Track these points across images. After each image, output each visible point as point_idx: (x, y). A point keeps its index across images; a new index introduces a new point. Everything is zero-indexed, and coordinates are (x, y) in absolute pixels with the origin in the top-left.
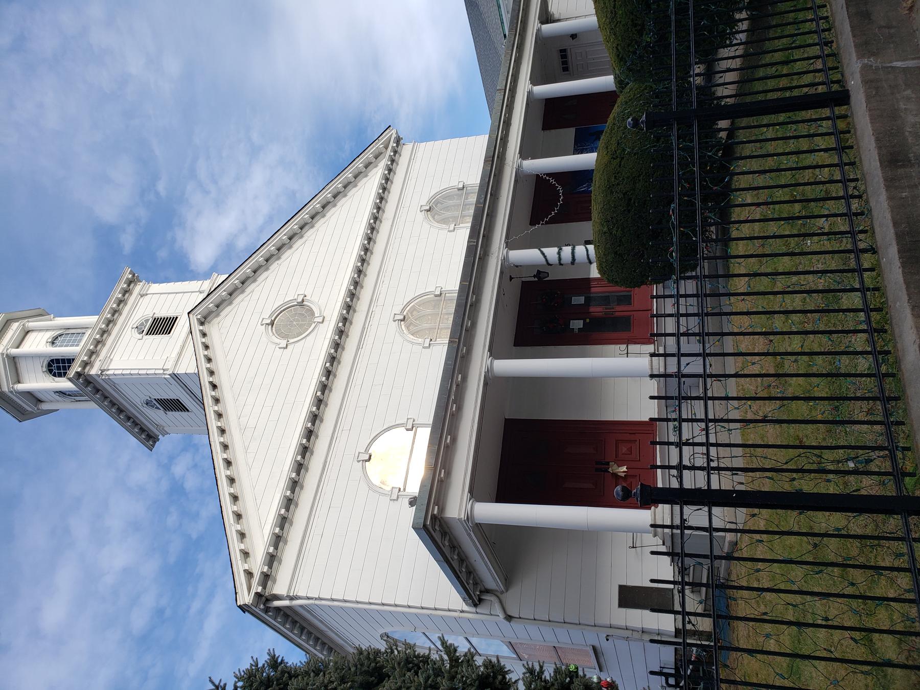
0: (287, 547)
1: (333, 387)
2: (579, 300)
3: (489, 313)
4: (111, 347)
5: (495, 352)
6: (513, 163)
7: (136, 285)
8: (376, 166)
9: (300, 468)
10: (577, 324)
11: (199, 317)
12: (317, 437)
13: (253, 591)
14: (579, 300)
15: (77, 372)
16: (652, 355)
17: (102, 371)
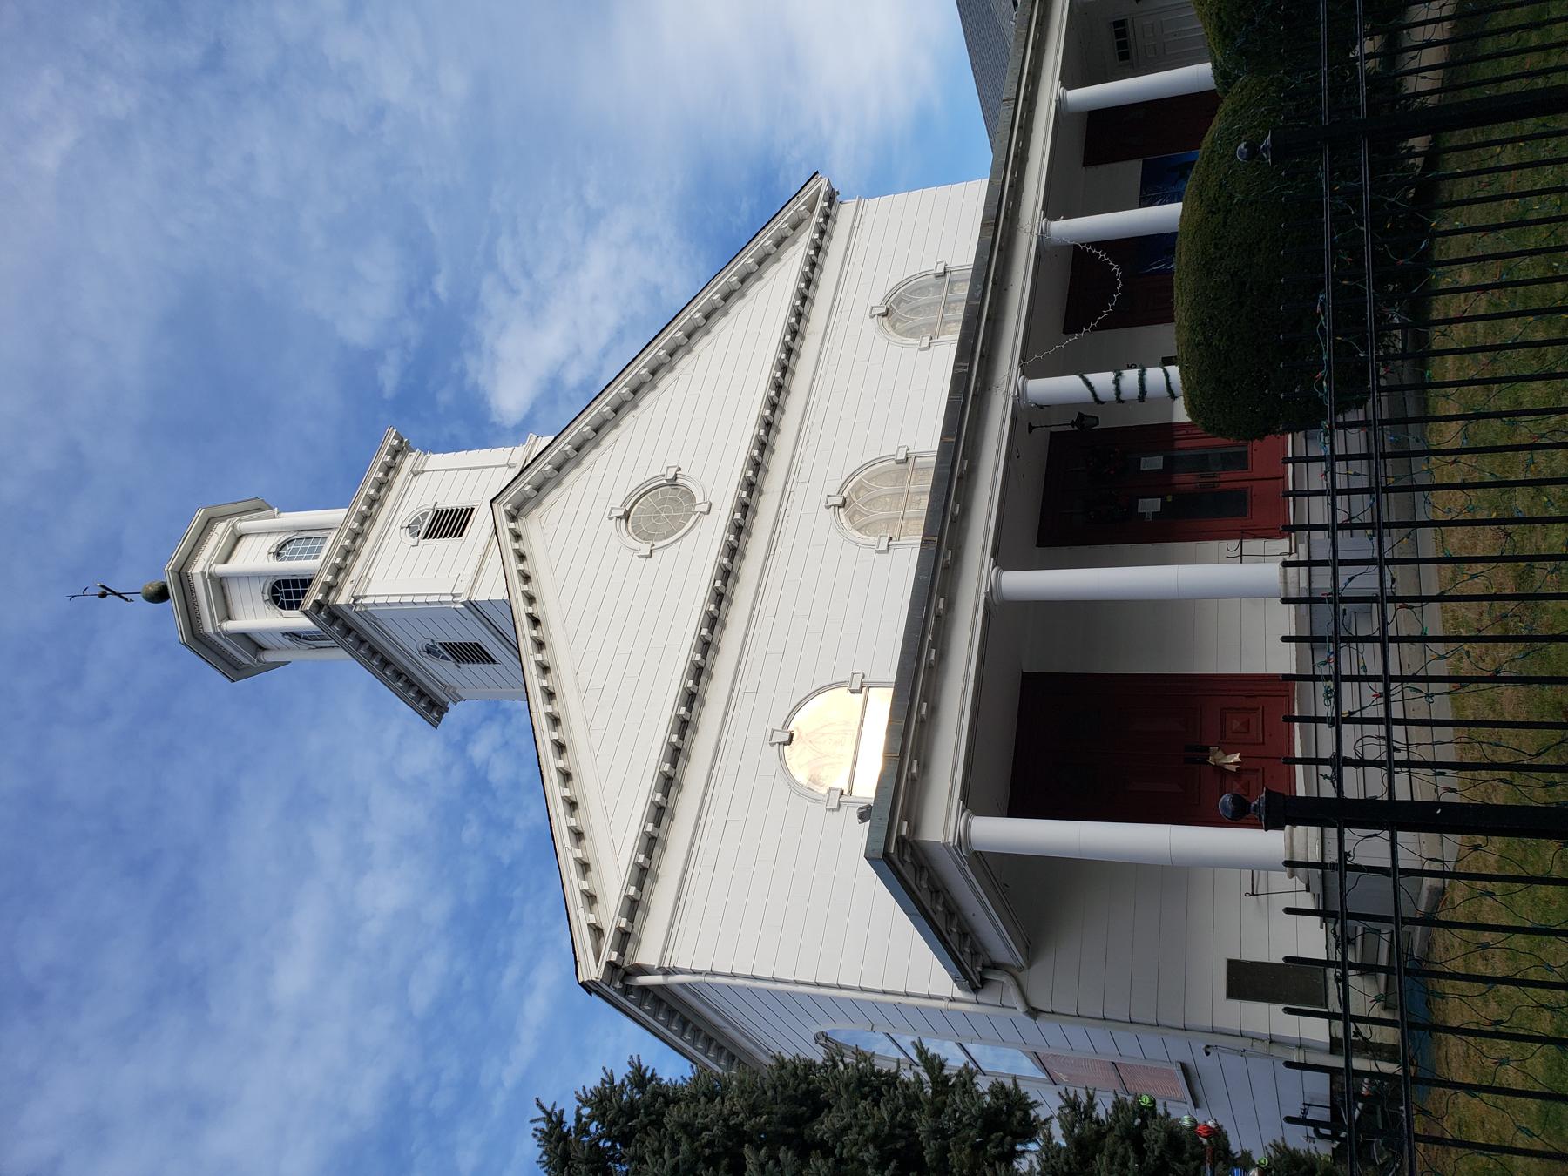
6: (1033, 226)
7: (405, 456)
8: (795, 243)
10: (1150, 506)
14: (1156, 462)
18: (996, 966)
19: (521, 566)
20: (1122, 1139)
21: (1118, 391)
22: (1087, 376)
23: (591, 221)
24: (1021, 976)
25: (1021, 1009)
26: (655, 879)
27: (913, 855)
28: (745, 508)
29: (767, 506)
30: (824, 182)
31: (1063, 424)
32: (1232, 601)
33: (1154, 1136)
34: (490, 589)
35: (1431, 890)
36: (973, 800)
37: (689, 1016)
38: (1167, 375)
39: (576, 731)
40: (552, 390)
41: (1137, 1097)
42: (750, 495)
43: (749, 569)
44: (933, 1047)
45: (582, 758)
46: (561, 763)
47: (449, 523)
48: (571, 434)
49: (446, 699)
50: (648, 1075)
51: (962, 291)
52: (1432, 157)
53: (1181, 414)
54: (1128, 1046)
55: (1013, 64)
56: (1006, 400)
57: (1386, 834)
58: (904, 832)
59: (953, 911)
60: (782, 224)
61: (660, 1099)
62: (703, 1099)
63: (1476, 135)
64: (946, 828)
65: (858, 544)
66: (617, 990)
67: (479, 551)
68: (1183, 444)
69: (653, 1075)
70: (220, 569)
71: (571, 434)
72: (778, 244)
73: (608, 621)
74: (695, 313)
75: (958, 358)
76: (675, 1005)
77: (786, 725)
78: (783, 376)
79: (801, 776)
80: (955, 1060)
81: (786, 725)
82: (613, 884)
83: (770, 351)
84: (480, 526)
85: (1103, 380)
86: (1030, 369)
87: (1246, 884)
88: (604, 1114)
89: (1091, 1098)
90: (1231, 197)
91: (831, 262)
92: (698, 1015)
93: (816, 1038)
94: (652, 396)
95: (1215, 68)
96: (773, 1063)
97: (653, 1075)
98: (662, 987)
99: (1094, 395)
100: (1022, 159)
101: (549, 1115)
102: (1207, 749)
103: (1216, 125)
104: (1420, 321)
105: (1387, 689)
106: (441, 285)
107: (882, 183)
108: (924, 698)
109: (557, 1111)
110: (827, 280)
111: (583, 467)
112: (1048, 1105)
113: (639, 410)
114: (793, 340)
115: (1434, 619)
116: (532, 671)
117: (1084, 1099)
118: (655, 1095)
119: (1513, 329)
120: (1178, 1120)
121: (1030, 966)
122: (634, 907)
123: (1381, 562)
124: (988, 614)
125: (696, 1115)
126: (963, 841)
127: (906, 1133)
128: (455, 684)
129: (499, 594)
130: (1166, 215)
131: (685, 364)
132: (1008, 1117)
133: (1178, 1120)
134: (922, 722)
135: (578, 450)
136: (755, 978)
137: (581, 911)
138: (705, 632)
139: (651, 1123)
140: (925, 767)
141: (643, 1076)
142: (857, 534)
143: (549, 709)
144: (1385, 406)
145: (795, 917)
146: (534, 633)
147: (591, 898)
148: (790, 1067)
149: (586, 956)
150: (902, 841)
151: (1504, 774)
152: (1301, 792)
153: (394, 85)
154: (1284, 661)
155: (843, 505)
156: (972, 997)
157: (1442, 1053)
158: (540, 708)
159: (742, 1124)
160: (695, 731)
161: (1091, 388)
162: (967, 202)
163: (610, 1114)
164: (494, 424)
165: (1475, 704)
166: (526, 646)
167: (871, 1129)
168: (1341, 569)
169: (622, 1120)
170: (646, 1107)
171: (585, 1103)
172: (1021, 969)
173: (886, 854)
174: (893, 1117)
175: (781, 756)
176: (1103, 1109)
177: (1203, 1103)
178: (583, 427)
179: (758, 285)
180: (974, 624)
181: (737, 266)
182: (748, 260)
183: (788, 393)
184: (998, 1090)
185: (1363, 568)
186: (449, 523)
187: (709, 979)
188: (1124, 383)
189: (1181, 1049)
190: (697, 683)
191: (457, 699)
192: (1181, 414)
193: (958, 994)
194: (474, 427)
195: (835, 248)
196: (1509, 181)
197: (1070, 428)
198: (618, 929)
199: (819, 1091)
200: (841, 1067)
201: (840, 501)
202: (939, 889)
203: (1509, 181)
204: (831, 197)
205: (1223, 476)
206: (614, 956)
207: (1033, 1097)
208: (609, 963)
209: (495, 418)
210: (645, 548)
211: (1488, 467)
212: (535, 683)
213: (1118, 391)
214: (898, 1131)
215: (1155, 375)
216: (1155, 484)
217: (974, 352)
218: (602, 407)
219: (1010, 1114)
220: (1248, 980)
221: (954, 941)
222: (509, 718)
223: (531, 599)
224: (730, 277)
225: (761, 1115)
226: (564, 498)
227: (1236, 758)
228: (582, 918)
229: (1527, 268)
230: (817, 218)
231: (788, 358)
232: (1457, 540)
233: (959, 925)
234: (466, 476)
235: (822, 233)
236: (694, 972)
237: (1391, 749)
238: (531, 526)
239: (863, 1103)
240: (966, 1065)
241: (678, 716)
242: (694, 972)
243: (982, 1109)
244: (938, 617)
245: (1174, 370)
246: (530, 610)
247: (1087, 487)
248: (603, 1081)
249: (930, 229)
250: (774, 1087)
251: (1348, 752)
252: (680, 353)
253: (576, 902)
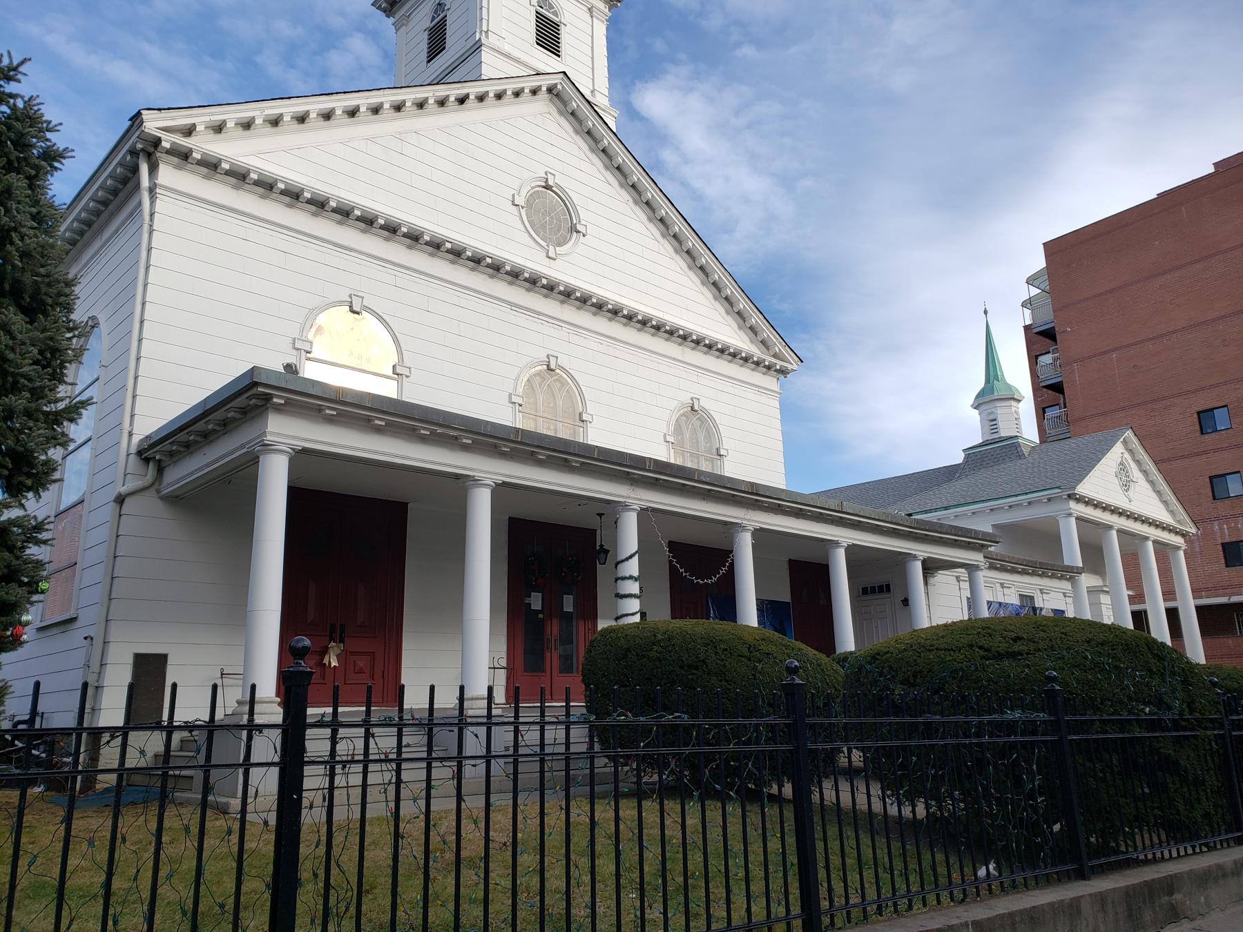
1: (319, 219)
2: (568, 604)
8: (752, 342)
14: (568, 604)
18: (160, 470)
19: (509, 93)
20: (8, 566)
21: (624, 578)
22: (637, 556)
23: (786, 181)
24: (153, 490)
25: (123, 490)
26: (236, 187)
27: (256, 407)
28: (551, 288)
29: (551, 306)
30: (795, 367)
31: (602, 539)
32: (460, 656)
33: (14, 592)
34: (491, 65)
35: (227, 805)
36: (301, 458)
37: (111, 207)
38: (633, 614)
39: (365, 128)
40: (658, 136)
41: (47, 579)
42: (560, 293)
43: (500, 288)
44: (87, 415)
45: (342, 130)
46: (339, 112)
47: (548, 35)
48: (616, 147)
49: (398, 15)
50: (56, 164)
51: (705, 467)
52: (778, 799)
53: (602, 625)
54: (91, 576)
55: (867, 510)
57: (277, 759)
58: (275, 400)
59: (208, 437)
60: (767, 333)
61: (33, 172)
62: (34, 210)
63: (790, 825)
64: (279, 434)
65: (517, 379)
66: (134, 144)
67: (524, 58)
68: (580, 628)
69: (56, 169)
71: (616, 147)
72: (752, 328)
73: (460, 164)
74: (705, 258)
75: (656, 461)
76: (121, 195)
77: (367, 309)
78: (653, 327)
79: (322, 319)
80: (77, 431)
81: (367, 309)
82: (231, 149)
83: (672, 317)
84: (543, 60)
85: (633, 567)
86: (645, 514)
87: (234, 662)
88: (17, 119)
89: (45, 542)
90: (760, 661)
91: (734, 369)
92: (112, 216)
93: (93, 318)
94: (643, 217)
95: (851, 653)
96: (70, 276)
97: (56, 169)
98: (138, 186)
99: (623, 561)
100: (799, 514)
101: (15, 69)
102: (342, 641)
103: (811, 652)
104: (664, 792)
105: (392, 760)
106: (748, 51)
107: (790, 413)
108: (389, 423)
109: (19, 76)
110: (723, 366)
111: (589, 153)
112: (36, 506)
113: (633, 205)
114: (679, 336)
115: (443, 805)
116: (420, 93)
117: (44, 536)
118: (38, 168)
119: (652, 853)
120: (27, 611)
121: (161, 498)
122: (211, 166)
123: (488, 758)
124: (457, 477)
125: (19, 202)
126: (267, 448)
127: (8, 386)
128: (411, 24)
129: (486, 72)
130: (749, 615)
131: (667, 247)
132: (27, 474)
133: (27, 611)
134: (369, 420)
135: (604, 151)
136: (147, 268)
137: (207, 119)
138: (448, 246)
139: (10, 162)
140: (330, 420)
141: (54, 159)
142: (525, 379)
143: (386, 106)
144: (603, 765)
145: (197, 305)
146: (452, 99)
147: (219, 128)
148: (67, 290)
150: (267, 398)
151: (324, 839)
152: (310, 711)
153: (904, 29)
154: (415, 699)
155: (549, 369)
156: (133, 450)
157: (90, 813)
158: (388, 98)
159: (12, 243)
160: (363, 231)
161: (627, 559)
162: (773, 476)
163: (18, 125)
164: (634, 84)
165: (379, 834)
166: (441, 91)
167: (11, 356)
168: (484, 729)
169: (12, 135)
170: (25, 159)
171: (29, 103)
172: (158, 491)
173: (256, 384)
174: (22, 376)
175: (340, 303)
176: (33, 551)
177: (42, 635)
178: (622, 157)
179: (723, 311)
181: (738, 295)
182: (743, 304)
183: (639, 330)
184: (50, 467)
185: (484, 744)
186: (548, 35)
187: (146, 227)
188: (629, 582)
189: (89, 619)
190: (405, 235)
191: (397, 27)
192: (602, 625)
193: (136, 439)
194: (630, 63)
195: (745, 373)
196: (756, 847)
197: (598, 544)
198: (191, 151)
199: (46, 315)
200: (69, 335)
201: (553, 367)
202: (227, 426)
203: (756, 847)
204: (783, 372)
205: (555, 655)
206: (166, 145)
207: (45, 495)
208: (159, 140)
209: (639, 85)
210: (520, 201)
211: (555, 840)
212: (410, 96)
213: (624, 578)
214: (10, 379)
215: (634, 605)
216: (552, 605)
217: (661, 473)
218: (637, 175)
219: (29, 475)
220: (149, 670)
221: (181, 437)
223: (481, 98)
224: (730, 289)
225: (21, 261)
226: (564, 135)
227: (334, 663)
228: (201, 119)
229: (696, 858)
230: (769, 360)
231: (666, 332)
232: (501, 820)
233: (196, 442)
234: (586, 56)
235: (757, 364)
236: (152, 215)
237: (344, 764)
238: (541, 106)
239: (36, 351)
240: (72, 440)
241: (377, 217)
242: (152, 215)
243: (32, 451)
244: (456, 438)
245: (637, 619)
246: (472, 97)
247: (551, 557)
248: (49, 122)
249: (753, 448)
250: (48, 276)
251: (342, 732)
252: (676, 244)
253: (216, 115)
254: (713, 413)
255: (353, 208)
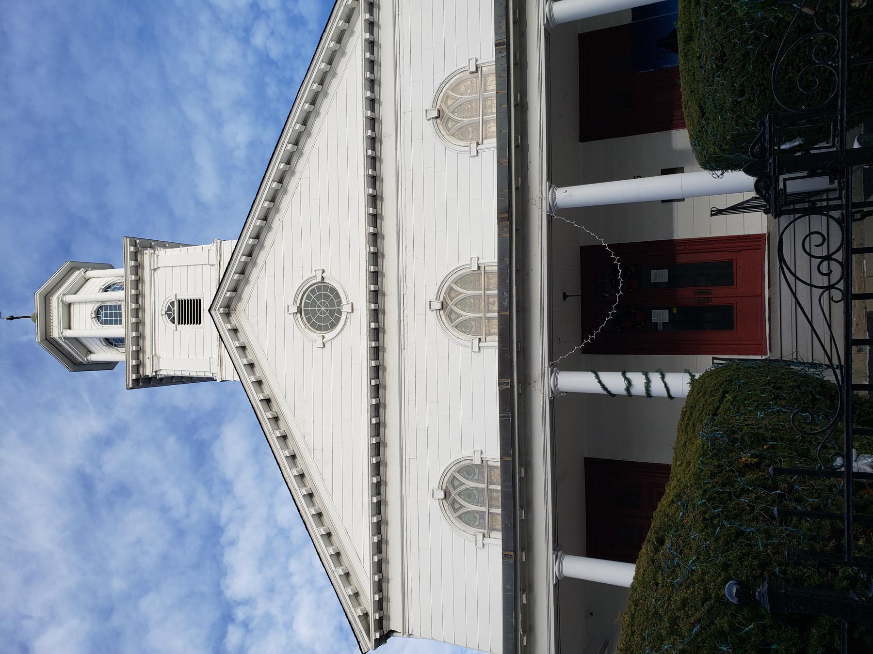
0: (387, 430)
1: (386, 309)
2: (660, 276)
3: (540, 56)
4: (151, 323)
5: (561, 547)
6: (541, 198)
7: (142, 255)
8: (352, 33)
9: (374, 180)
10: (660, 316)
11: (221, 310)
12: (379, 27)
13: (373, 638)
14: (660, 276)
15: (133, 380)
16: (765, 565)
17: (156, 372)
56: (544, 398)
70: (69, 298)
83: (359, 133)
124: (552, 402)
131: (301, 166)
149: (363, 636)
180: (548, 607)
190: (372, 53)
222: (268, 16)
238: (244, 315)
252: (295, 158)
254: (437, 85)
255: (368, 157)
